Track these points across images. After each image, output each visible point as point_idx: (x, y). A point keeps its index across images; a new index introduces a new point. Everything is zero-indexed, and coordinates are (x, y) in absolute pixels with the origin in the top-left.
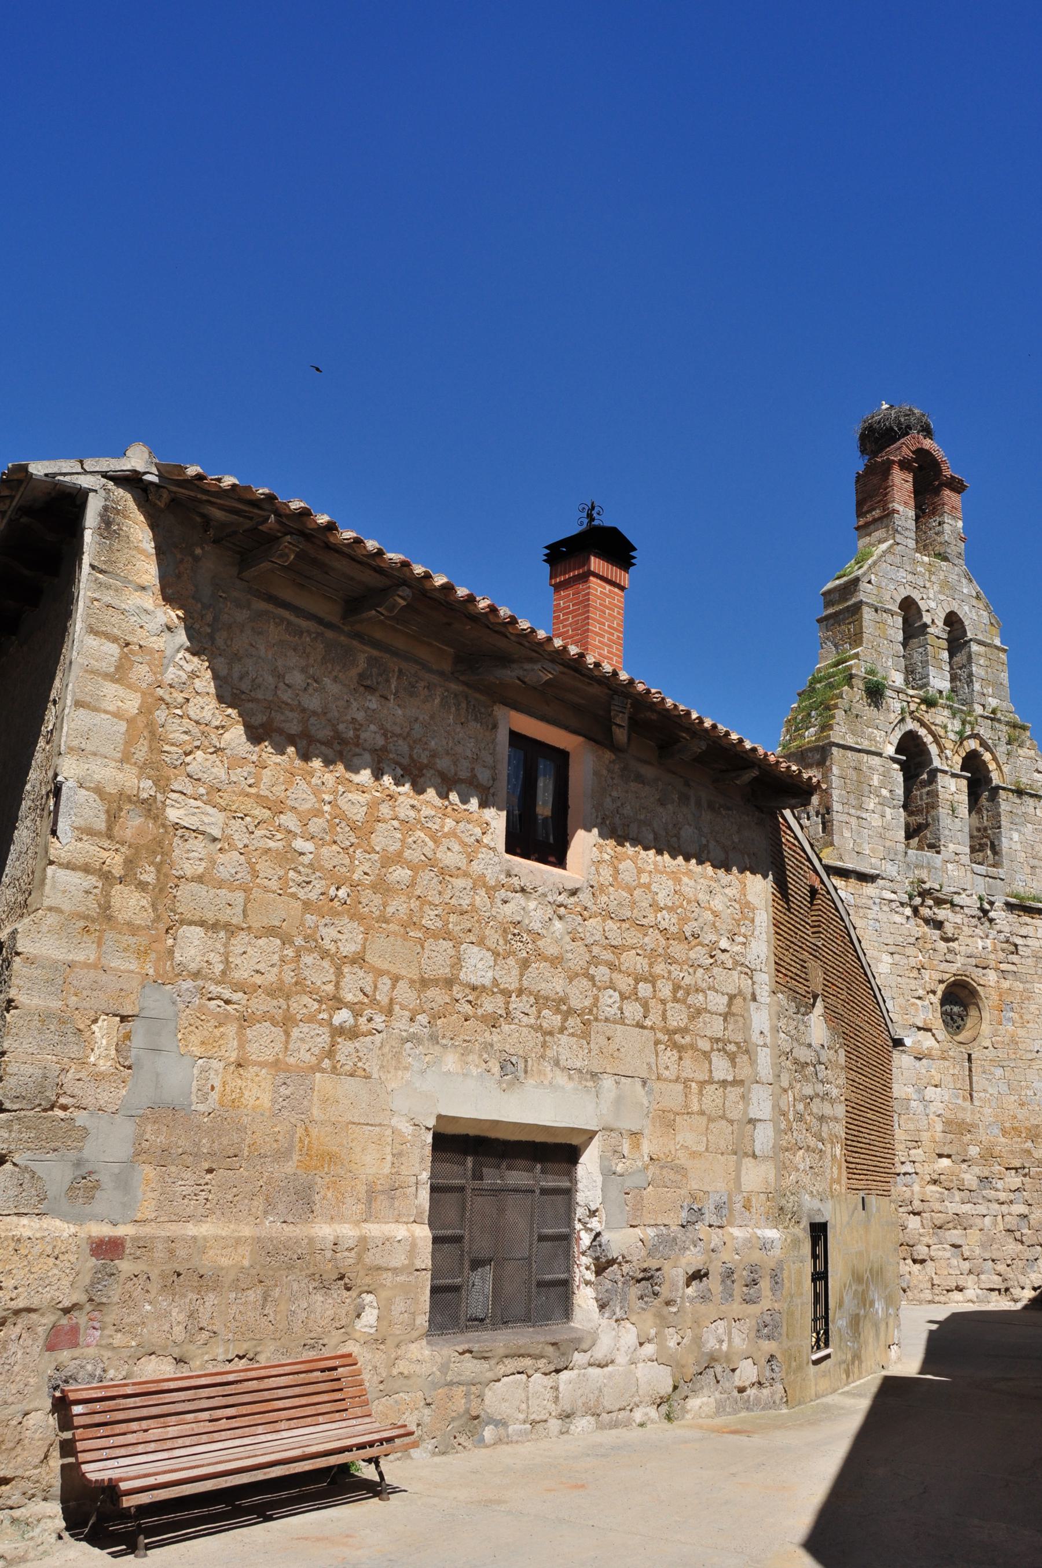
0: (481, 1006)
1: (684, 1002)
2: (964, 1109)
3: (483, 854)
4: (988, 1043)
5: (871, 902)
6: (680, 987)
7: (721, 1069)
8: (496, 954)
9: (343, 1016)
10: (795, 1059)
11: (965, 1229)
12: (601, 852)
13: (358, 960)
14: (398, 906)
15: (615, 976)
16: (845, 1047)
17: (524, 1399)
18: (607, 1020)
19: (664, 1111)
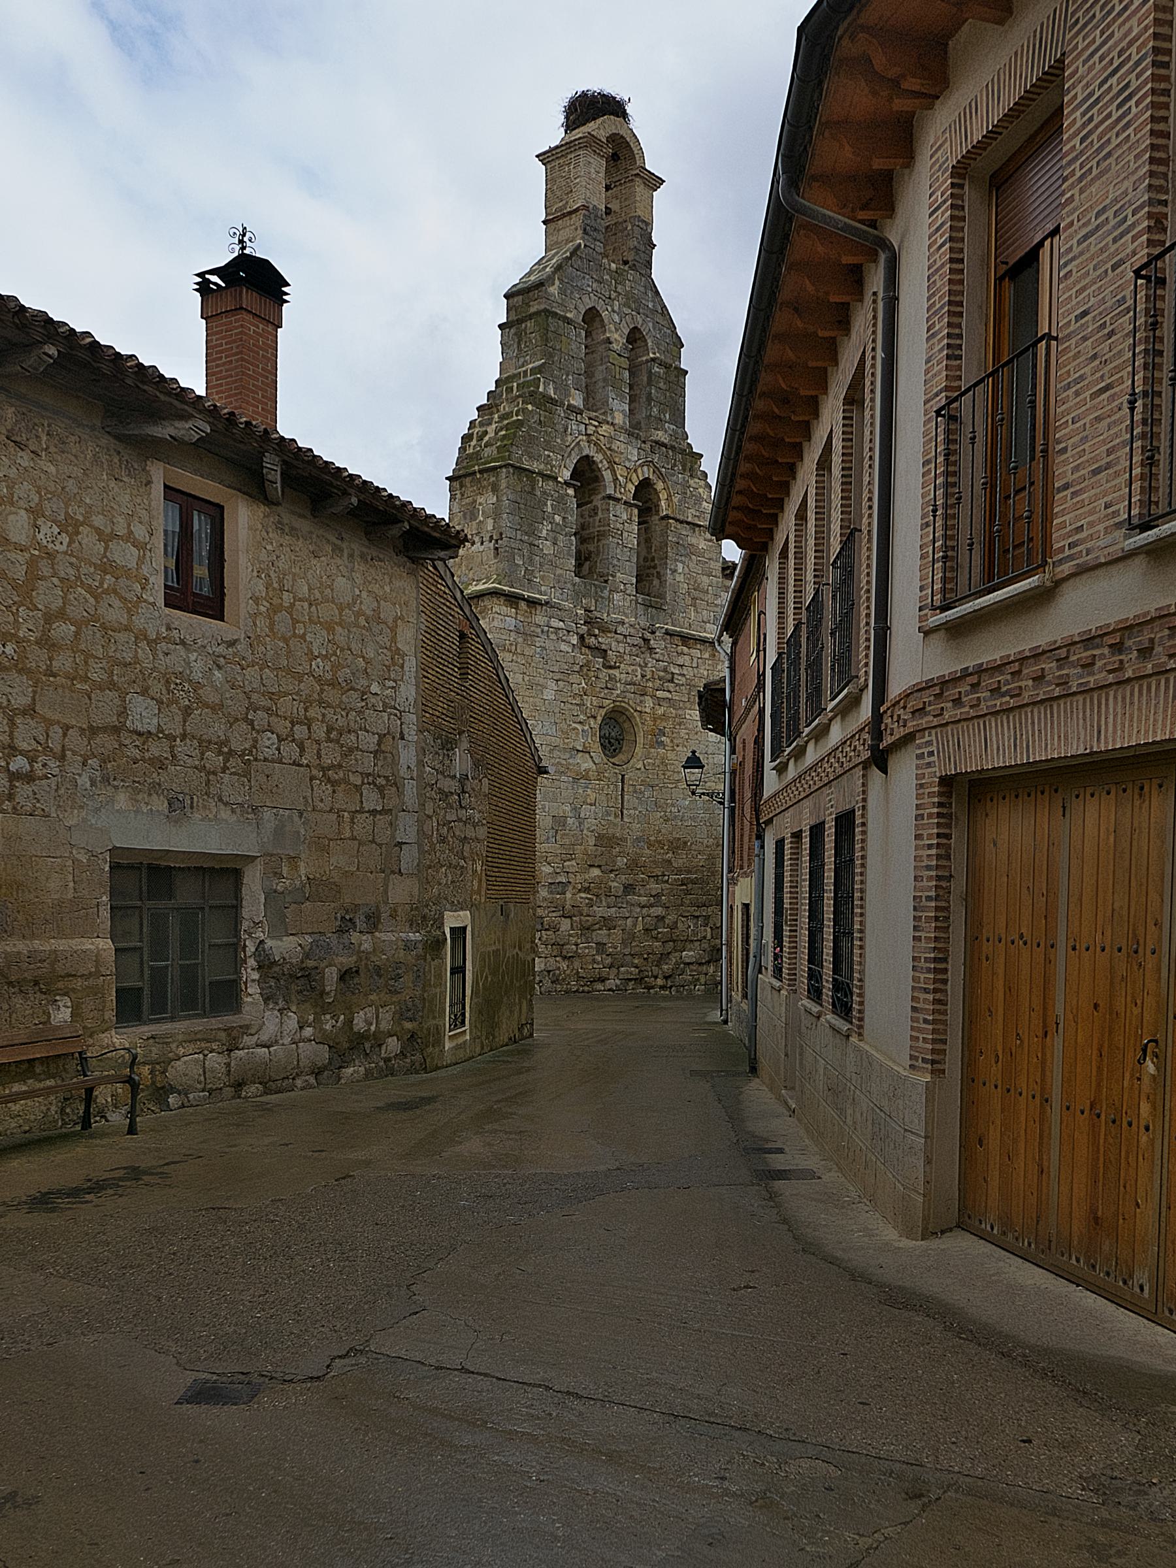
0: (148, 750)
1: (338, 741)
2: (615, 825)
3: (143, 609)
4: (640, 765)
5: (539, 630)
6: (333, 729)
7: (371, 800)
8: (160, 702)
9: (19, 763)
10: (440, 789)
11: (610, 929)
12: (257, 605)
13: (30, 711)
14: (63, 662)
15: (273, 719)
16: (489, 777)
17: (202, 1073)
18: (265, 760)
19: (319, 838)
